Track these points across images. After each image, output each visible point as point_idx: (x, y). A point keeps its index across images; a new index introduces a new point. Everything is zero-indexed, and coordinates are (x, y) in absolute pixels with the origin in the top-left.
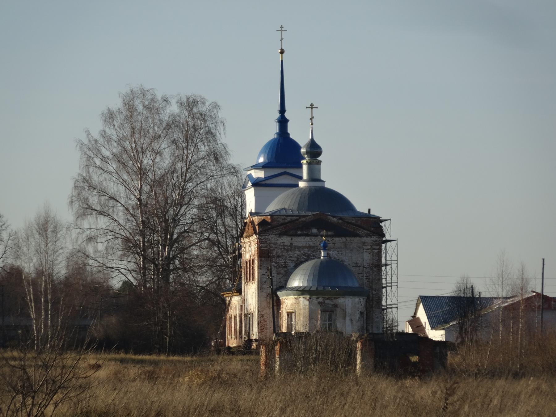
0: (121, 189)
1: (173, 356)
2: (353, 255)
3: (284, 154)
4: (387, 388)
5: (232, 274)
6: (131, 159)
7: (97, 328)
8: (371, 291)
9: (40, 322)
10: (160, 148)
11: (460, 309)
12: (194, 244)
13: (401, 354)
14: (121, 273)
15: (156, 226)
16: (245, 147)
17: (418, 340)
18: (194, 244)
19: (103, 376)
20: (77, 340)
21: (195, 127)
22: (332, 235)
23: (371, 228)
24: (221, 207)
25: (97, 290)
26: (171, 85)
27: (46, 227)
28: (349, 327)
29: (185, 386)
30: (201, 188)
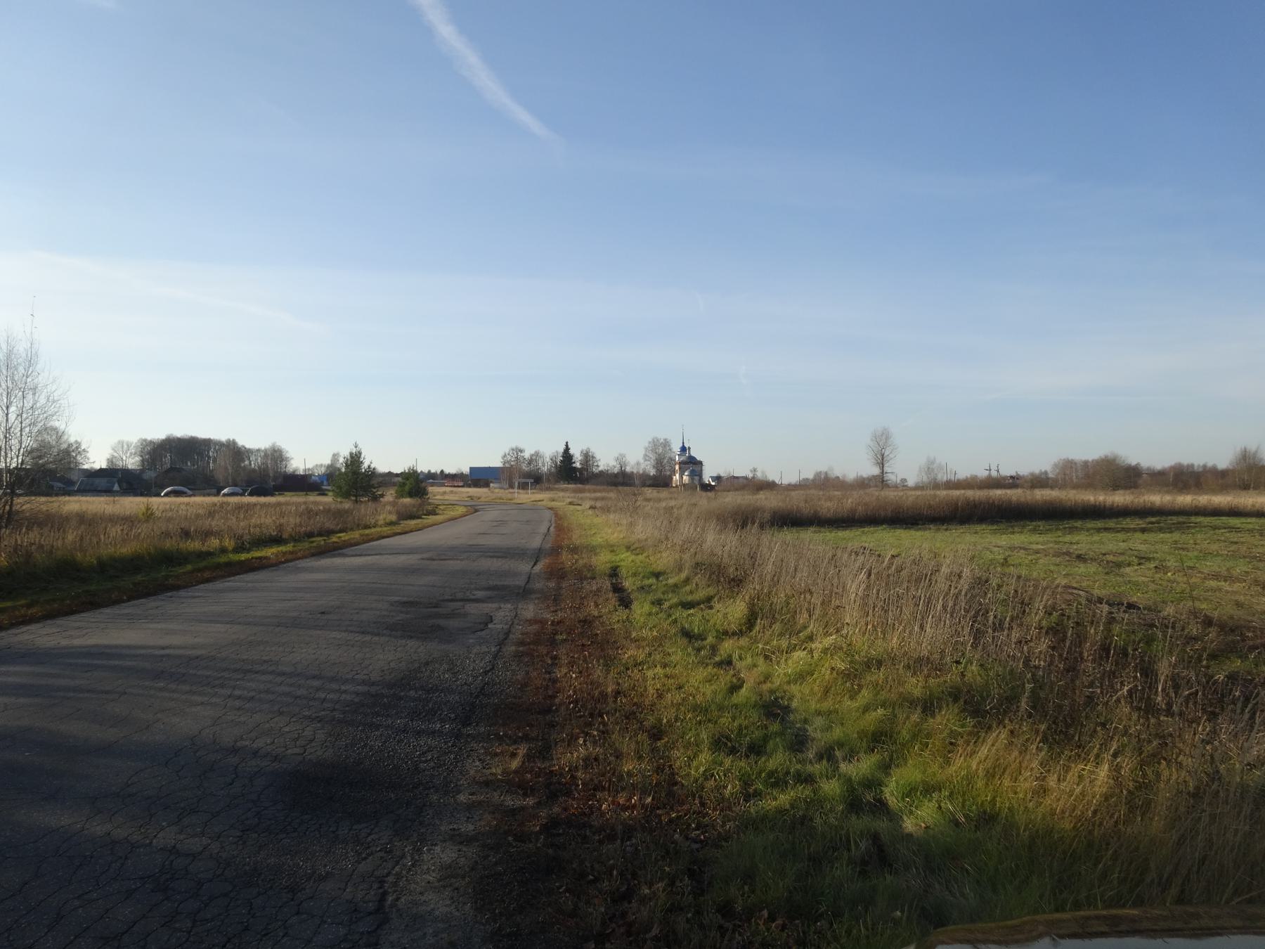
0: (653, 456)
1: (918, 497)
2: (697, 468)
3: (683, 449)
4: (704, 494)
5: (674, 472)
6: (654, 450)
7: (648, 483)
8: (700, 476)
9: (637, 482)
10: (659, 450)
11: (718, 478)
12: (370, 914)
13: (706, 487)
14: (652, 472)
15: (659, 463)
16: (676, 448)
17: (709, 485)
18: (370, 914)
19: (650, 492)
20: (644, 485)
21: (666, 444)
22: (693, 464)
23: (700, 463)
24: (672, 459)
25: (648, 476)
26: (662, 436)
27: (638, 464)
28: (696, 482)
29: (664, 493)
30: (668, 456)
